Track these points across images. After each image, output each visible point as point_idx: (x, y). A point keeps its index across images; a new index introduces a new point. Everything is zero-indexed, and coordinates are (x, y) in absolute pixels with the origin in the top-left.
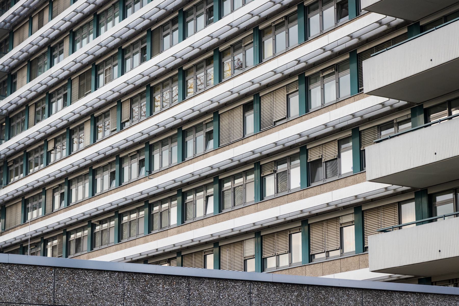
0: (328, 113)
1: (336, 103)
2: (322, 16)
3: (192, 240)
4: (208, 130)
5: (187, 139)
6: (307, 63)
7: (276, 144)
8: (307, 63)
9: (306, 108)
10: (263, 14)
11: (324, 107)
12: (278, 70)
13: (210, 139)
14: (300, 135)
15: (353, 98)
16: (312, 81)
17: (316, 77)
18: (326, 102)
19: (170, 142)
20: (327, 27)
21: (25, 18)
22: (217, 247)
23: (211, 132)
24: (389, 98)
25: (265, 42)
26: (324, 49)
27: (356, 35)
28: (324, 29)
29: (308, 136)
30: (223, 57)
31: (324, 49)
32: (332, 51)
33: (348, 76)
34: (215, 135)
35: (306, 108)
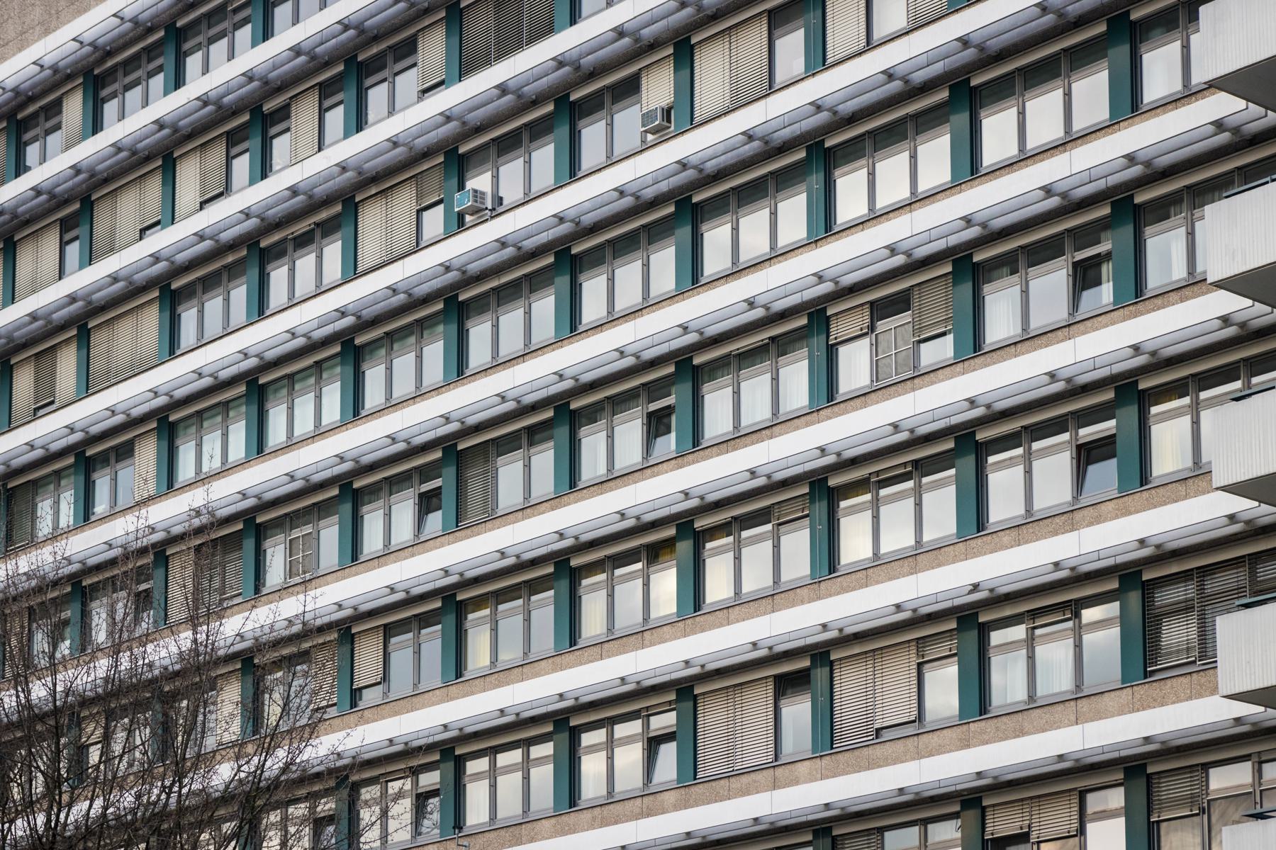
0: (1069, 343)
1: (1069, 325)
2: (528, 313)
3: (561, 696)
4: (426, 487)
5: (267, 544)
6: (638, 357)
7: (503, 553)
8: (577, 380)
9: (353, 552)
10: (179, 394)
11: (389, 553)
12: (511, 395)
13: (429, 511)
14: (687, 494)
15: (961, 365)
16: (366, 498)
17: (373, 491)
18: (617, 466)
19: (524, 441)
20: (539, 337)
21: (148, 159)
22: (562, 731)
23: (437, 492)
24: (1254, 300)
25: (181, 448)
26: (622, 353)
27: (762, 300)
28: (501, 354)
29: (702, 498)
30: (94, 471)
31: (622, 353)
32: (837, 283)
33: (550, 454)
34: (449, 498)
35: (353, 552)
